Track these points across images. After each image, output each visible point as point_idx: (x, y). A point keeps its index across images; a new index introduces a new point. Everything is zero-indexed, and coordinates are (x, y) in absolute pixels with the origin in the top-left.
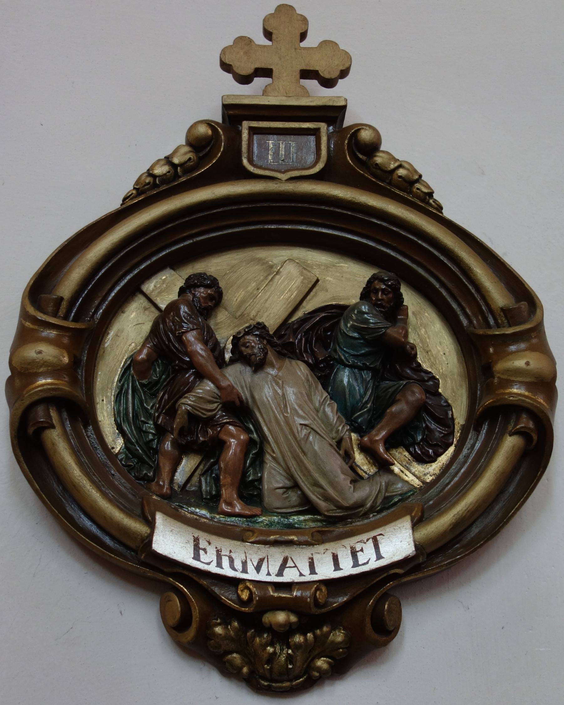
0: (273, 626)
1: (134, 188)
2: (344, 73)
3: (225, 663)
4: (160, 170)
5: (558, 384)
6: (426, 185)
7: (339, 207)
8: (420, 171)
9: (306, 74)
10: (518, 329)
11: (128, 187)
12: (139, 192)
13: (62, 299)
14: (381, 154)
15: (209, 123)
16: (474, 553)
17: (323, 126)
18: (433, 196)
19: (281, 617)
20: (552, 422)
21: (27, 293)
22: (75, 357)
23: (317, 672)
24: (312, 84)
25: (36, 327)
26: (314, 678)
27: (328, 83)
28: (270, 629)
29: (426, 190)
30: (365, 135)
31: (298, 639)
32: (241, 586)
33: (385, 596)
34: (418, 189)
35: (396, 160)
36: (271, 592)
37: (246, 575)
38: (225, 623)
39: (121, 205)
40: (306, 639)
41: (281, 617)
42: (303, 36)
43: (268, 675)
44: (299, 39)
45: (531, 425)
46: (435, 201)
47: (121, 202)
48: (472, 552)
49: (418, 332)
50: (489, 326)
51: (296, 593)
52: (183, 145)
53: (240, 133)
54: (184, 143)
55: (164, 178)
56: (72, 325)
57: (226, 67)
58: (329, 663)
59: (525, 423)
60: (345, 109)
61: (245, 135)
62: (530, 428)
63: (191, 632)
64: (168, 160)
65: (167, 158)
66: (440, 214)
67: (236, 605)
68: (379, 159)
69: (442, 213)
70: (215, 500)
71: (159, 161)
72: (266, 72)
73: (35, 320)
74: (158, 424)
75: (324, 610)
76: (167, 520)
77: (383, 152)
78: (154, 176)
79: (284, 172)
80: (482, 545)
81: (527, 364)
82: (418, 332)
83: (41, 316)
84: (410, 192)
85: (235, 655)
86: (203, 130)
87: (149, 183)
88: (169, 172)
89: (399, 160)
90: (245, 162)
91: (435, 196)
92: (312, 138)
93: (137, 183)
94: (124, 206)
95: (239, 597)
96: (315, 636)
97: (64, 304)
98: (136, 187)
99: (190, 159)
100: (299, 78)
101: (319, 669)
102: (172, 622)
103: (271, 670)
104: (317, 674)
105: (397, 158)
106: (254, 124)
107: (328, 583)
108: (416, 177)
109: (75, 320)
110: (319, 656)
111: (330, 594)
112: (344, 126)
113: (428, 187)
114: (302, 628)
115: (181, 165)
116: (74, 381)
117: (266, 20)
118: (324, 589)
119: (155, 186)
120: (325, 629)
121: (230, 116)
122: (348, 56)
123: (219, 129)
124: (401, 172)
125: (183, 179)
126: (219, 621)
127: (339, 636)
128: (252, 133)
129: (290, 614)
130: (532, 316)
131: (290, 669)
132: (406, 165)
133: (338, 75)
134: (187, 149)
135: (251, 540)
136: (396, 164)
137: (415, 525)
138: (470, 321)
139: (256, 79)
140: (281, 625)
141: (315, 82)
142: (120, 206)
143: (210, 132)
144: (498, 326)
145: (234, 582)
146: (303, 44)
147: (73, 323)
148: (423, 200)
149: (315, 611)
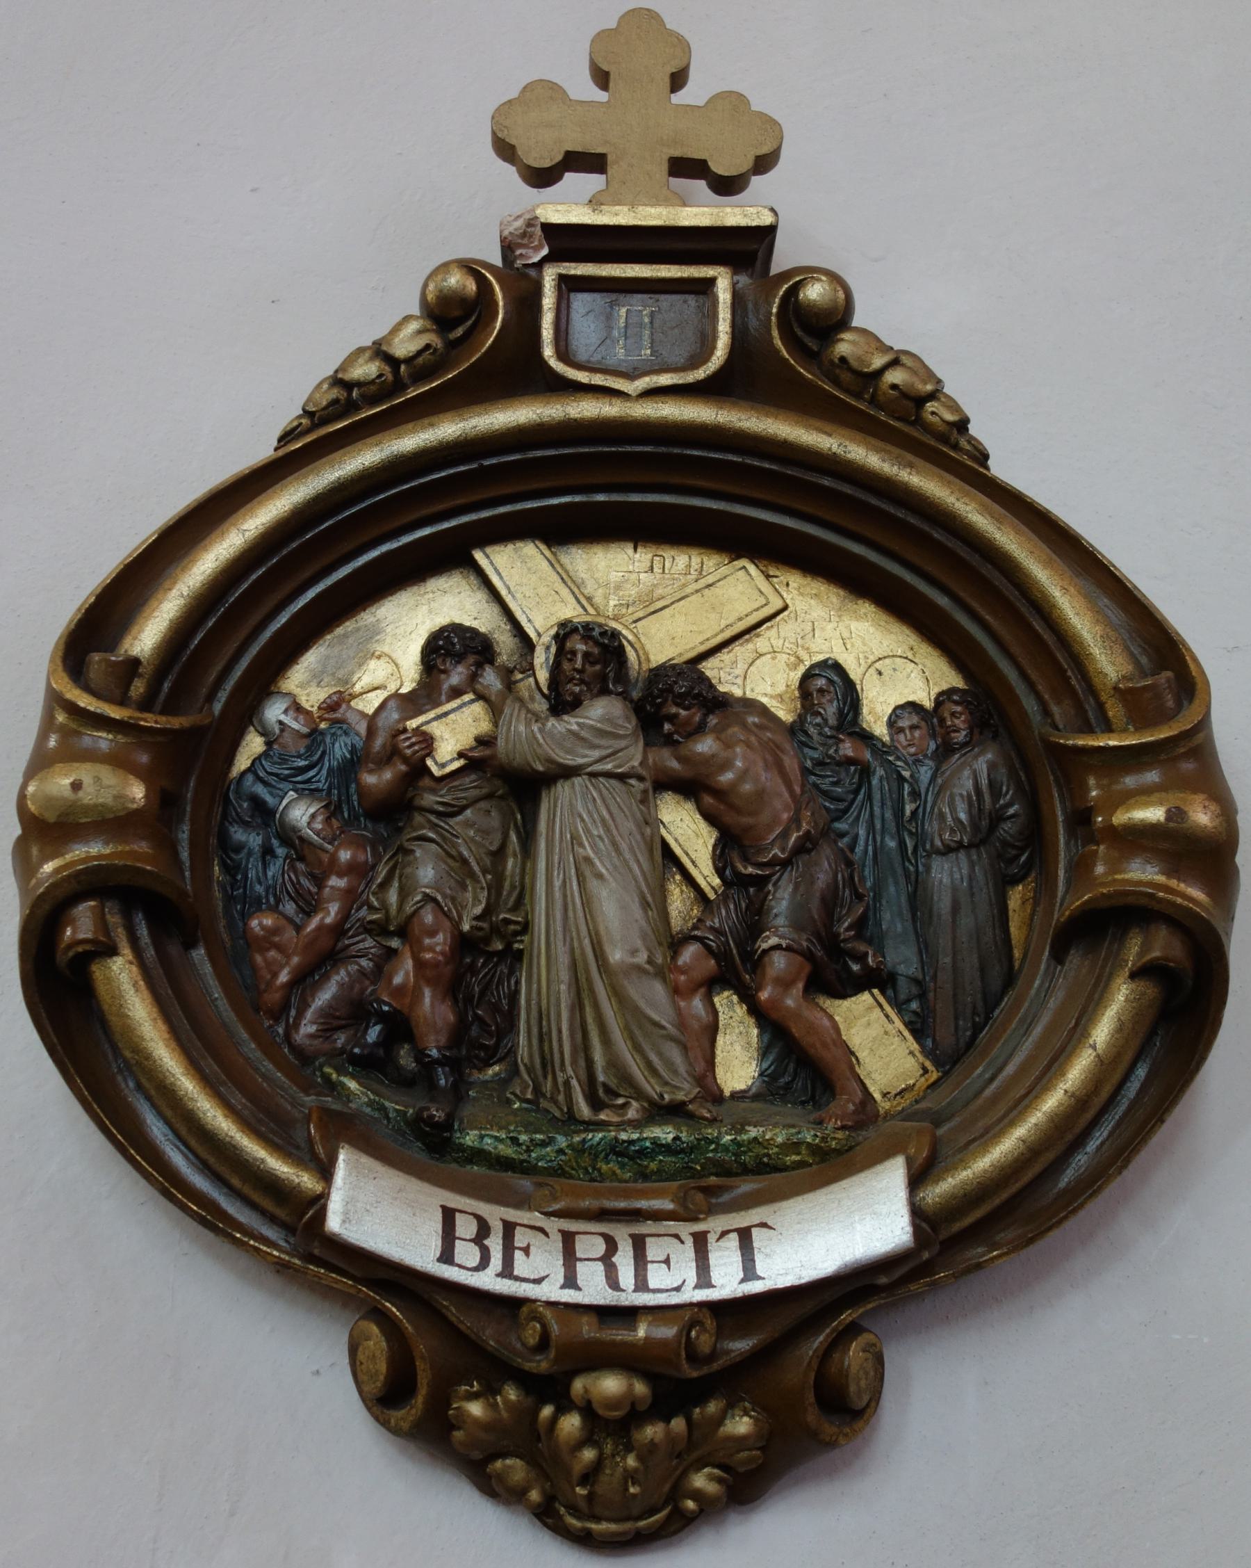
0: (595, 1405)
2: (764, 164)
3: (490, 1477)
4: (367, 370)
8: (939, 375)
11: (288, 413)
13: (135, 662)
14: (847, 336)
15: (470, 267)
18: (967, 429)
23: (694, 1499)
26: (688, 1515)
27: (727, 186)
28: (588, 1411)
29: (950, 417)
30: (814, 292)
31: (652, 1432)
33: (853, 1330)
35: (885, 349)
38: (489, 1392)
39: (276, 449)
40: (668, 1433)
41: (611, 1384)
42: (678, 80)
43: (583, 1505)
44: (668, 85)
46: (972, 440)
47: (275, 444)
49: (811, 1165)
54: (416, 310)
55: (375, 391)
56: (150, 721)
57: (505, 150)
58: (720, 1481)
60: (770, 237)
61: (548, 301)
64: (379, 351)
65: (377, 344)
66: (985, 472)
68: (845, 347)
69: (987, 468)
71: (361, 351)
72: (592, 162)
73: (73, 710)
74: (654, 1405)
77: (857, 329)
78: (348, 386)
79: (630, 376)
82: (811, 1165)
83: (85, 701)
86: (455, 280)
89: (892, 348)
90: (548, 352)
91: (973, 429)
94: (281, 453)
99: (428, 347)
101: (697, 1495)
102: (375, 1387)
104: (690, 1504)
105: (888, 342)
108: (929, 387)
109: (166, 711)
110: (699, 1465)
112: (771, 274)
113: (954, 406)
114: (660, 1408)
115: (409, 360)
116: (168, 846)
117: (601, 37)
118: (709, 1323)
119: (349, 407)
120: (712, 1407)
122: (771, 125)
124: (895, 377)
125: (412, 393)
127: (741, 1425)
130: (1185, 703)
131: (634, 1496)
132: (904, 359)
137: (916, 1181)
138: (1046, 712)
139: (569, 177)
140: (613, 1403)
143: (471, 286)
145: (513, 1304)
146: (677, 98)
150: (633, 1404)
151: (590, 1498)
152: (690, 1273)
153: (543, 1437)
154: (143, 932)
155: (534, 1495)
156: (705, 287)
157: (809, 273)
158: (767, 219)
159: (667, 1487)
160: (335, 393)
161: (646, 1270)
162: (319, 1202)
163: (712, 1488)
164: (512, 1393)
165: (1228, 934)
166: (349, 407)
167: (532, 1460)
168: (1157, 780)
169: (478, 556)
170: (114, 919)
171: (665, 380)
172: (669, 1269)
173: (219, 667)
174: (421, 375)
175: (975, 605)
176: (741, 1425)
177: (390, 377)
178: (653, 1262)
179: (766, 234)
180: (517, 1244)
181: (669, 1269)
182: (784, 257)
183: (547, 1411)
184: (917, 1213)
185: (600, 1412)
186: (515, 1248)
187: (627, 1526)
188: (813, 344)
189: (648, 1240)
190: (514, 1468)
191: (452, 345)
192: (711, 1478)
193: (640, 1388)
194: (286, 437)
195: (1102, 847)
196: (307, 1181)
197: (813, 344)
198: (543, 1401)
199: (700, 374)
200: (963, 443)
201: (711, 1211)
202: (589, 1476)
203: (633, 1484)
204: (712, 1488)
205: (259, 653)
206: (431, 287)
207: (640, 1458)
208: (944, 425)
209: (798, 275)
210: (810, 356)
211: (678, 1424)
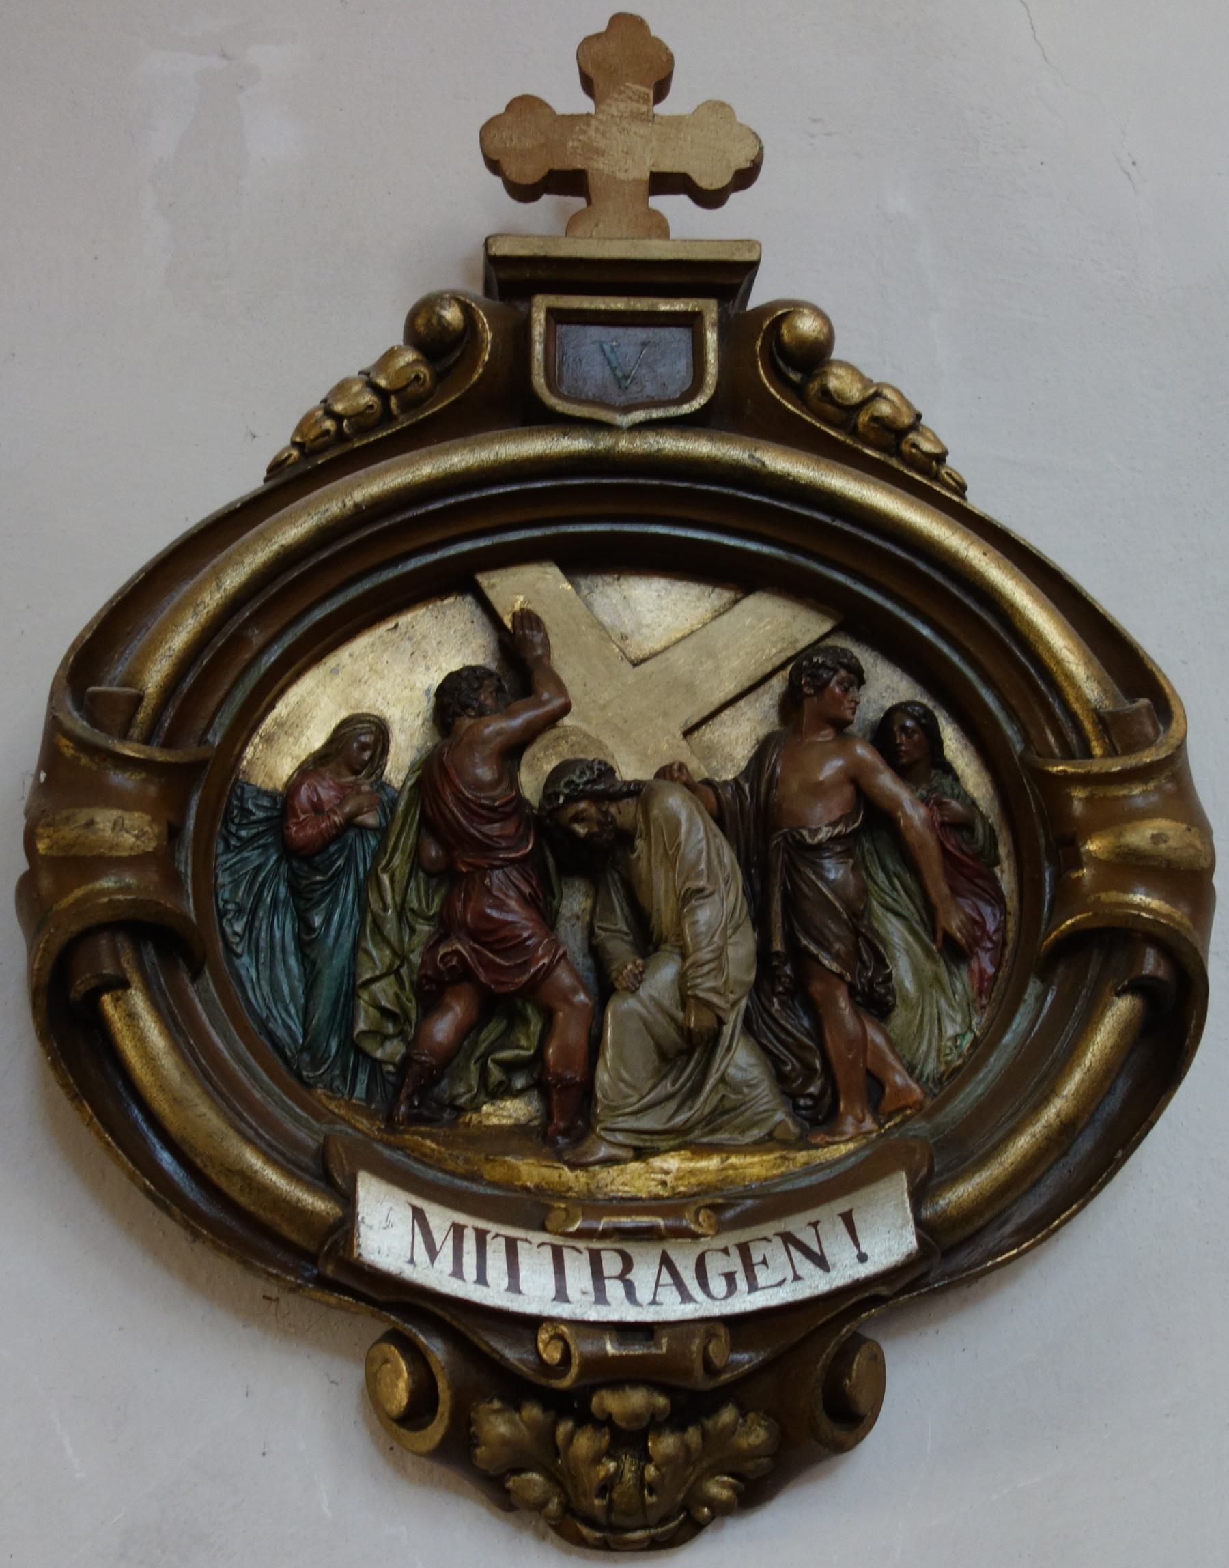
1: (294, 444)
2: (745, 177)
5: (1217, 881)
6: (932, 438)
8: (919, 407)
9: (663, 183)
10: (1131, 761)
12: (306, 450)
16: (1044, 1245)
17: (710, 309)
18: (945, 461)
24: (675, 207)
25: (726, 1164)
27: (710, 199)
28: (606, 1422)
30: (807, 325)
31: (665, 1445)
37: (566, 1306)
39: (266, 480)
41: (637, 1399)
42: (661, 90)
43: (602, 1518)
47: (264, 474)
48: (1044, 1239)
55: (362, 421)
56: (160, 755)
58: (731, 1487)
59: (1151, 964)
61: (538, 330)
63: (436, 1430)
69: (964, 498)
70: (416, 1103)
75: (725, 1377)
77: (842, 364)
78: (338, 418)
79: (626, 409)
85: (535, 1476)
87: (327, 432)
90: (539, 380)
91: (950, 460)
93: (299, 430)
96: (705, 1435)
98: (298, 439)
100: (647, 193)
101: (711, 1503)
107: (734, 1322)
109: (167, 744)
111: (735, 1346)
112: (752, 304)
113: (936, 441)
114: (677, 1420)
116: (173, 880)
118: (722, 1331)
120: (727, 1415)
128: (552, 321)
131: (652, 1505)
132: (888, 393)
133: (730, 183)
134: (410, 356)
137: (919, 1195)
141: (683, 200)
145: (533, 1323)
146: (661, 109)
149: (701, 1381)
150: (653, 1416)
151: (610, 1508)
153: (562, 1452)
155: (553, 1506)
157: (793, 308)
159: (680, 1497)
160: (329, 424)
162: (346, 1225)
163: (725, 1494)
165: (1206, 952)
167: (552, 1477)
169: (483, 580)
171: (656, 414)
173: (221, 694)
178: (610, 1278)
180: (606, 1273)
183: (564, 1428)
184: (920, 1225)
186: (604, 1278)
188: (795, 377)
189: (751, 1245)
191: (439, 377)
192: (724, 1485)
193: (661, 1401)
194: (276, 468)
195: (1085, 871)
197: (795, 377)
199: (686, 409)
202: (606, 1487)
203: (651, 1494)
204: (725, 1494)
206: (420, 321)
207: (657, 1468)
208: (923, 457)
209: (781, 309)
210: (798, 392)
211: (693, 1435)
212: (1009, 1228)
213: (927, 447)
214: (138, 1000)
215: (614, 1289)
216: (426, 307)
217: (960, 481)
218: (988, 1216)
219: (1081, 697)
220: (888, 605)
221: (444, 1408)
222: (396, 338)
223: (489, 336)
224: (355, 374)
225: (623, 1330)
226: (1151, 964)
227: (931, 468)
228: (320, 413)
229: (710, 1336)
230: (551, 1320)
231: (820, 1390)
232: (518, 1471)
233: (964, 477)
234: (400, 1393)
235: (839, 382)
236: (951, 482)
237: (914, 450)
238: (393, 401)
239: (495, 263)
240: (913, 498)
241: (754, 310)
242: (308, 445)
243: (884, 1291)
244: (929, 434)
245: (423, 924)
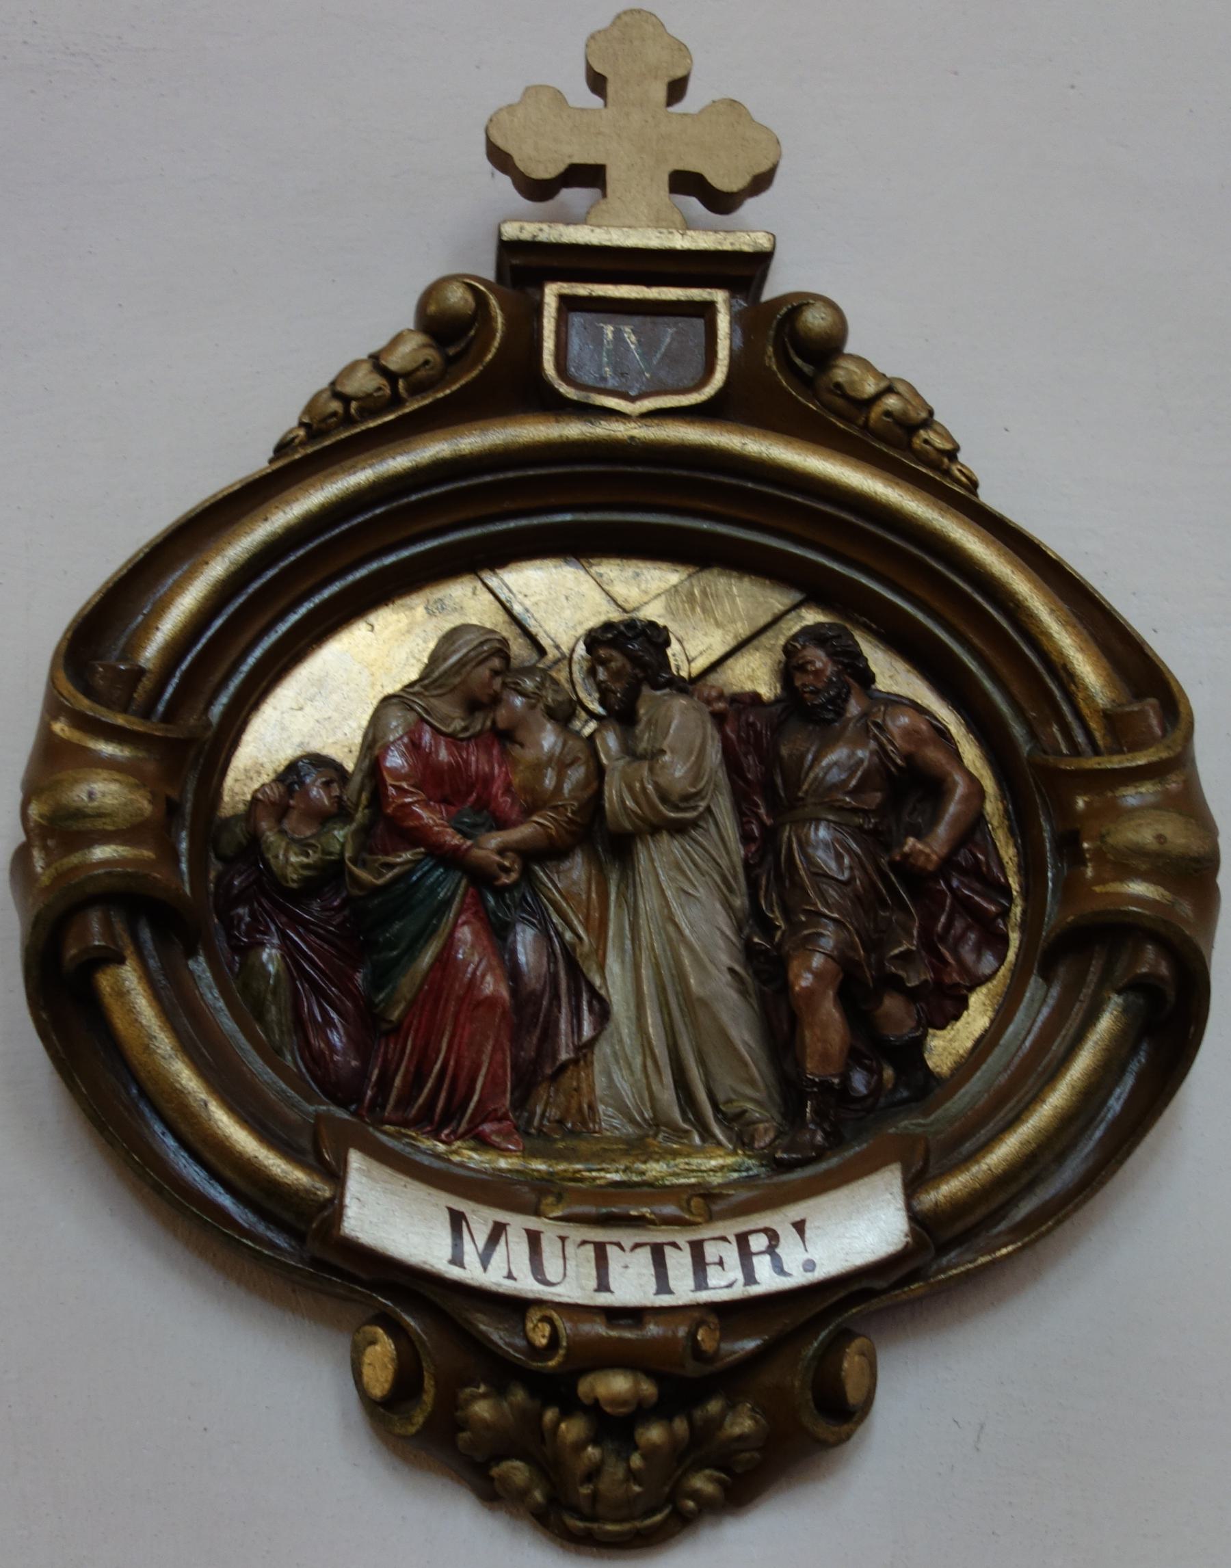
0: (602, 1403)
1: (302, 424)
2: (761, 182)
4: (365, 382)
6: (943, 432)
7: (336, 524)
13: (141, 672)
14: (843, 363)
17: (719, 296)
19: (617, 1384)
20: (1207, 960)
21: (61, 661)
22: (169, 801)
23: (693, 1500)
28: (594, 1410)
30: (815, 319)
31: (654, 1434)
32: (534, 1315)
33: (845, 1336)
34: (926, 442)
36: (600, 1329)
38: (499, 1391)
39: (271, 461)
41: (617, 1384)
42: (677, 89)
45: (1164, 969)
47: (271, 454)
50: (1075, 751)
51: (653, 1329)
52: (410, 331)
53: (537, 310)
54: (410, 324)
55: (371, 405)
57: (499, 158)
58: (719, 1482)
59: (1150, 962)
62: (1161, 978)
66: (973, 498)
67: (518, 1353)
69: (976, 495)
76: (408, 1186)
77: (851, 356)
78: (345, 399)
80: (1049, 1231)
81: (1160, 838)
84: (908, 448)
86: (457, 296)
87: (334, 414)
88: (379, 389)
91: (961, 457)
92: (699, 323)
93: (310, 408)
95: (531, 1344)
97: (146, 683)
98: (306, 420)
99: (426, 362)
101: (695, 1495)
103: (595, 1497)
104: (691, 1504)
106: (723, 322)
108: (924, 415)
110: (698, 1466)
113: (948, 437)
115: (406, 375)
118: (713, 1320)
119: (347, 420)
120: (714, 1407)
121: (514, 268)
123: (491, 297)
124: (891, 402)
126: (482, 1389)
127: (742, 1424)
129: (641, 1376)
132: (900, 388)
134: (417, 340)
135: (551, 1215)
136: (883, 384)
137: (913, 1186)
140: (617, 1401)
142: (266, 464)
144: (1097, 752)
146: (677, 108)
147: (162, 726)
148: (936, 466)
149: (692, 1369)
152: (735, 1272)
154: (146, 934)
155: (538, 1495)
156: (706, 310)
158: (763, 242)
159: (667, 1489)
160: (336, 406)
161: (705, 1271)
162: (335, 1207)
164: (519, 1396)
165: (1210, 945)
166: (347, 420)
168: (580, 855)
170: (119, 927)
172: (723, 1269)
174: (417, 389)
175: (963, 627)
176: (742, 1424)
177: (388, 391)
179: (760, 261)
180: (709, 1259)
181: (723, 1269)
182: (777, 285)
183: (550, 1415)
184: (915, 1217)
185: (608, 1409)
187: (626, 1527)
188: (807, 369)
190: (517, 1471)
191: (449, 361)
192: (711, 1479)
193: (648, 1388)
194: (282, 448)
196: (325, 1191)
197: (807, 369)
198: (546, 1404)
200: (955, 470)
201: (711, 1218)
202: (593, 1474)
205: (989, 612)
207: (645, 1457)
210: (807, 383)
211: (680, 1426)
212: (1002, 1227)
213: (939, 442)
214: (129, 975)
215: (762, 1266)
216: (432, 292)
217: (969, 474)
218: (981, 1211)
219: (1090, 698)
220: (920, 616)
221: (428, 1397)
222: (407, 319)
223: (500, 320)
224: (364, 356)
225: (614, 1314)
226: (1150, 962)
227: (942, 462)
228: (326, 395)
229: (700, 1323)
230: (539, 1303)
231: (809, 1396)
232: (499, 1458)
233: (976, 473)
234: (379, 1378)
235: (842, 373)
236: (963, 479)
237: (928, 447)
238: (401, 383)
239: (508, 249)
240: (911, 486)
241: (767, 303)
242: (315, 426)
243: (880, 1284)
244: (938, 428)
245: (446, 894)
